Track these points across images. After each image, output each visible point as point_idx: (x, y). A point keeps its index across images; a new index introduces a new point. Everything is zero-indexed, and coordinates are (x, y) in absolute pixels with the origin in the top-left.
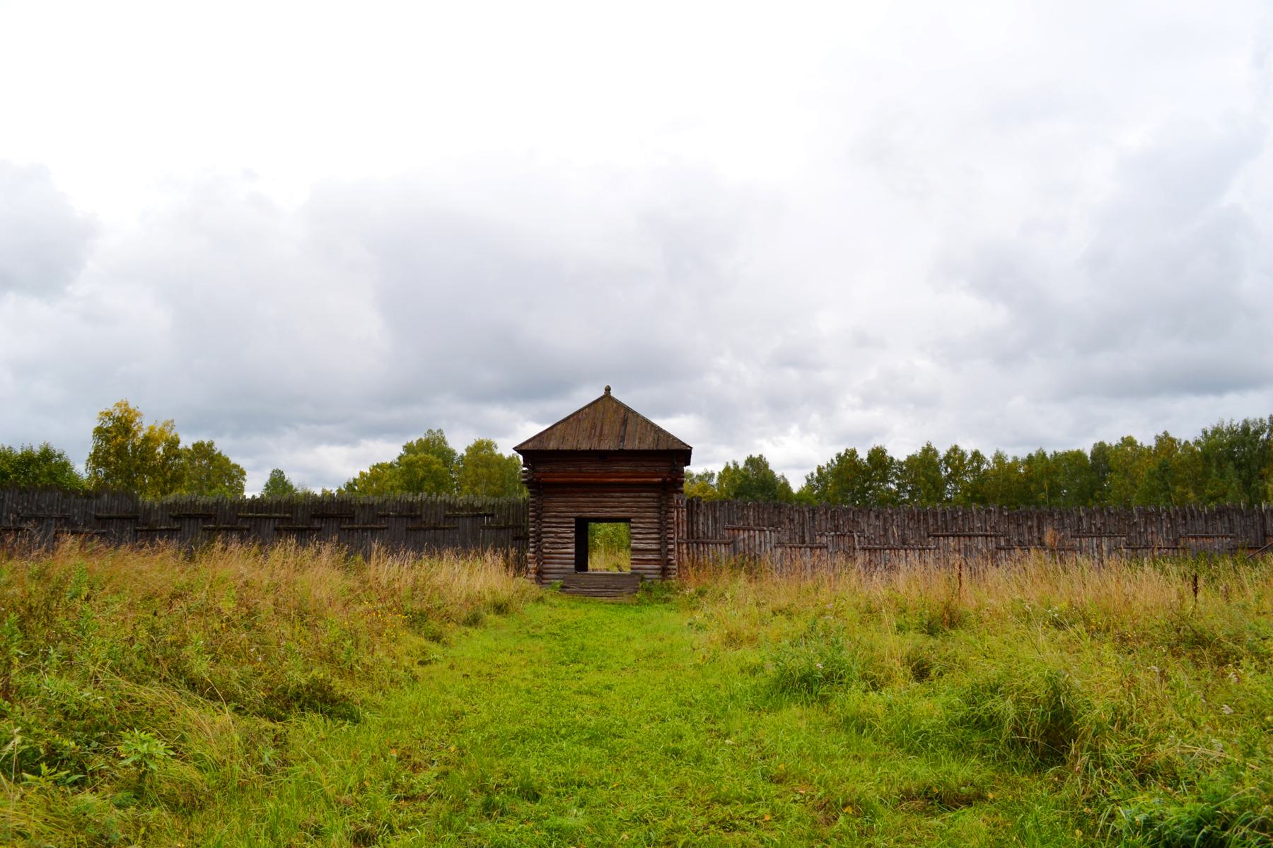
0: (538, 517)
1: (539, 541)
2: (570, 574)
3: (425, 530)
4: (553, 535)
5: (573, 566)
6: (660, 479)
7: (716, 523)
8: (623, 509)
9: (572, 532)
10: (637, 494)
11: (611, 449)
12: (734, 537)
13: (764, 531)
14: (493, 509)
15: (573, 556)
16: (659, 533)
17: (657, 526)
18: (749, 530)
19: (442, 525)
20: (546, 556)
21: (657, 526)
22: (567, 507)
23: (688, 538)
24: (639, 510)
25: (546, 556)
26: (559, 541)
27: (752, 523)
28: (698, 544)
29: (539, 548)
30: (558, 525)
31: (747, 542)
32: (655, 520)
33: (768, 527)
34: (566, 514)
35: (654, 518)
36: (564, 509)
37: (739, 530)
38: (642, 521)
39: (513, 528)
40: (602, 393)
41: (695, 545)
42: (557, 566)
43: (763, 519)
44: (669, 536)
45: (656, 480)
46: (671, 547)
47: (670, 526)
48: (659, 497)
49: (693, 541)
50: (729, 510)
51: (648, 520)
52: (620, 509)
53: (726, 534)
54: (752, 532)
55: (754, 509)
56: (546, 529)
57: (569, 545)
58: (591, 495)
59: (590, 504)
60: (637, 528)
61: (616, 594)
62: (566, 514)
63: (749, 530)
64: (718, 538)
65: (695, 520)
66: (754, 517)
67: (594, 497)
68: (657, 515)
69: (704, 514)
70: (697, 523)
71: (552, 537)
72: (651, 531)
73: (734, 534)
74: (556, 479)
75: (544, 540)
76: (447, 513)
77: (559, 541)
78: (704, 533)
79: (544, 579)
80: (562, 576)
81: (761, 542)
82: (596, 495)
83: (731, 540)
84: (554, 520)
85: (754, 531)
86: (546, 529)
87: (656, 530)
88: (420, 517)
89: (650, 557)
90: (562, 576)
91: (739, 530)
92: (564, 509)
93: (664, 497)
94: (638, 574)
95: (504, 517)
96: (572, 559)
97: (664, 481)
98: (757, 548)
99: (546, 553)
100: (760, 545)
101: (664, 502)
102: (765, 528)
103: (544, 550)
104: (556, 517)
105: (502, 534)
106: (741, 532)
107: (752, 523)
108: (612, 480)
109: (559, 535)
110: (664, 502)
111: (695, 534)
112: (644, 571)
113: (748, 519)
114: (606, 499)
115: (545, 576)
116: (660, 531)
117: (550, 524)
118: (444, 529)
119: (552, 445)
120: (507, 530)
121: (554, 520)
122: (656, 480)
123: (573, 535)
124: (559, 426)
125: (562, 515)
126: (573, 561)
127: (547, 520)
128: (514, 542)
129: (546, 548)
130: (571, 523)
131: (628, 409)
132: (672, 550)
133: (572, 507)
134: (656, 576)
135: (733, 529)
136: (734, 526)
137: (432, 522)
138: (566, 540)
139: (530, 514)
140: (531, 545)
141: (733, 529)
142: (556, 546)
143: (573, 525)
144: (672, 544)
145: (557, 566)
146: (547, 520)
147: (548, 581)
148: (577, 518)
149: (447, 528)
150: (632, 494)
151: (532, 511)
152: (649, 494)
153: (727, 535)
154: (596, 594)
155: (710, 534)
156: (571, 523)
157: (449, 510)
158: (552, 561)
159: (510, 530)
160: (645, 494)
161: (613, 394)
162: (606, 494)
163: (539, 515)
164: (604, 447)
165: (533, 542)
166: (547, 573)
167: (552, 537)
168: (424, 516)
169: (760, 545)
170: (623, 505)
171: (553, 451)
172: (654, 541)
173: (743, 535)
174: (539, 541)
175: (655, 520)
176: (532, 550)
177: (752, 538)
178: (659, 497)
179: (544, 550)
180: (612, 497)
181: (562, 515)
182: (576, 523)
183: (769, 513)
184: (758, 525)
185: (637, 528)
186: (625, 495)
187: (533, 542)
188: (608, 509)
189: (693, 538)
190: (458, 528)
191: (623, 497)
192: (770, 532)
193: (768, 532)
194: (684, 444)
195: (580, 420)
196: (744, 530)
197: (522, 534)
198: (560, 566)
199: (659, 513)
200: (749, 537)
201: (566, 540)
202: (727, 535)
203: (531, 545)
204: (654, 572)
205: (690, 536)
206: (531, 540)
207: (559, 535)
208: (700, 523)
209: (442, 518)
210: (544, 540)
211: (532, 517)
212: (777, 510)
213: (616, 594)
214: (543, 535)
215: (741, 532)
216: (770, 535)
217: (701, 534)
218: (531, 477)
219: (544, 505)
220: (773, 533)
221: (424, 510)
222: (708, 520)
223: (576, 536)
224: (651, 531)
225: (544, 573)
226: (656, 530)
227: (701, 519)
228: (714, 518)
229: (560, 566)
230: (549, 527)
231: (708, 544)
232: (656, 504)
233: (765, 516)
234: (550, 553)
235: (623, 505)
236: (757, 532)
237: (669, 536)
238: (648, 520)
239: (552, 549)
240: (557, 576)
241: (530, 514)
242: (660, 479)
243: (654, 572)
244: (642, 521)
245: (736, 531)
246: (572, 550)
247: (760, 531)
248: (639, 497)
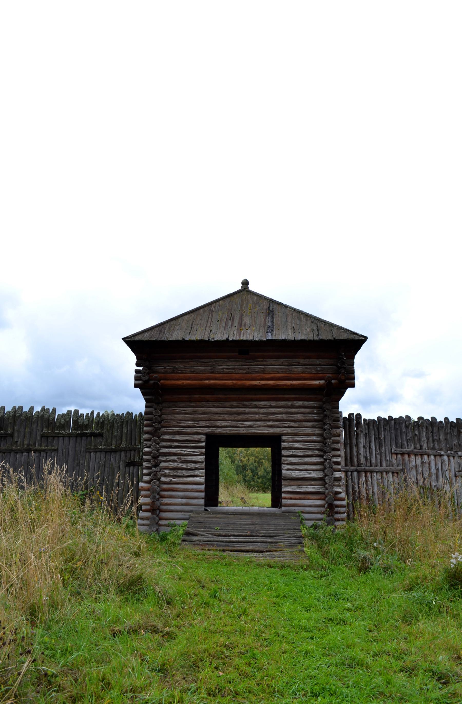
0: (154, 433)
1: (156, 466)
2: (198, 512)
3: (16, 452)
4: (175, 458)
5: (202, 502)
6: (322, 382)
7: (381, 446)
8: (271, 423)
9: (201, 454)
10: (290, 403)
11: (256, 339)
12: (404, 464)
13: (441, 455)
14: (102, 427)
15: (203, 487)
16: (321, 456)
17: (318, 446)
18: (422, 455)
19: (37, 447)
20: (165, 486)
21: (318, 446)
22: (193, 420)
23: (346, 465)
24: (292, 424)
25: (165, 486)
26: (183, 466)
27: (425, 446)
28: (359, 472)
29: (155, 475)
30: (182, 444)
31: (420, 470)
32: (315, 438)
33: (446, 451)
34: (194, 430)
35: (314, 435)
36: (191, 423)
37: (409, 455)
38: (298, 438)
39: (126, 452)
40: (238, 287)
41: (355, 474)
42: (179, 500)
43: (439, 441)
44: (334, 459)
45: (317, 382)
46: (337, 475)
47: (335, 446)
48: (320, 407)
49: (352, 468)
50: (396, 430)
51: (305, 438)
52: (268, 423)
53: (393, 459)
54: (426, 457)
55: (427, 428)
56: (165, 450)
57: (198, 479)
58: (228, 404)
59: (226, 417)
60: (291, 448)
61: (269, 547)
62: (194, 430)
63: (422, 455)
64: (384, 464)
65: (354, 442)
66: (428, 439)
67: (231, 407)
68: (318, 431)
69: (365, 435)
70: (357, 445)
71: (174, 461)
72: (310, 453)
73: (403, 460)
74: (181, 382)
75: (163, 464)
76: (45, 431)
77: (183, 466)
78: (366, 459)
79: (161, 519)
80: (187, 515)
81: (437, 470)
82: (234, 403)
83: (401, 467)
84: (177, 437)
85: (429, 455)
86: (165, 450)
87: (316, 452)
88: (12, 435)
89: (309, 489)
90: (187, 515)
91: (409, 455)
92: (191, 423)
93: (326, 406)
94: (295, 513)
95: (116, 437)
96: (285, 448)
97: (329, 384)
98: (434, 477)
99: (165, 483)
100: (437, 474)
101: (327, 412)
102: (443, 453)
103: (163, 479)
104: (179, 433)
105: (112, 459)
106: (413, 457)
107: (425, 446)
108: (257, 382)
109: (183, 458)
110: (327, 412)
111: (355, 460)
112: (302, 509)
113: (420, 440)
114: (248, 410)
115: (163, 515)
116: (323, 452)
117: (171, 443)
118: (40, 451)
119: (177, 335)
120: (118, 454)
121: (177, 437)
122: (317, 382)
123: (202, 458)
124: (186, 317)
125: (188, 430)
126: (203, 494)
127: (167, 437)
128: (127, 469)
129: (166, 476)
130: (199, 441)
131: (272, 301)
132: (339, 479)
133: (201, 420)
134: (319, 516)
135: (403, 454)
136: (404, 450)
137: (26, 442)
138: (193, 465)
139: (145, 429)
140: (145, 471)
141: (403, 454)
142: (178, 473)
143: (203, 444)
144: (339, 471)
145: (179, 500)
146: (167, 437)
147: (166, 522)
148: (206, 434)
149: (44, 451)
150: (282, 403)
151: (147, 426)
152: (306, 403)
153: (394, 461)
154: (238, 547)
155: (374, 460)
156: (199, 441)
157: (47, 427)
158: (349, 458)
159: (123, 453)
160: (300, 403)
161: (251, 287)
162: (247, 403)
163: (157, 430)
164: (247, 336)
165: (147, 468)
166: (314, 407)
167: (174, 461)
168: (16, 435)
169: (437, 474)
170: (271, 417)
171: (177, 342)
172: (314, 467)
173: (415, 461)
174: (156, 466)
175: (315, 438)
176: (146, 478)
177: (427, 465)
178: (320, 407)
179: (163, 479)
180: (256, 407)
181: (188, 430)
182: (207, 441)
183: (446, 434)
184: (434, 448)
185: (291, 448)
186: (273, 404)
187: (147, 468)
188: (251, 423)
189: (352, 466)
190: (57, 450)
191: (271, 407)
192: (448, 456)
193: (446, 458)
194: (356, 334)
195: (213, 311)
196: (416, 455)
197: (137, 459)
198: (184, 501)
199: (322, 428)
200: (423, 463)
201: (193, 465)
202: (394, 461)
203: (145, 471)
204: (316, 509)
205: (349, 464)
206: (145, 464)
207: (183, 458)
208: (361, 446)
209: (38, 438)
210: (163, 464)
211: (147, 433)
212: (456, 430)
213: (269, 547)
214: (161, 458)
215: (413, 457)
216: (449, 460)
217: (363, 460)
218: (147, 378)
219: (164, 417)
220: (452, 458)
221: (16, 428)
222: (370, 442)
223: (207, 460)
224: (310, 453)
225: (161, 511)
226: (316, 452)
227: (362, 441)
228: (378, 439)
229: (184, 501)
230: (170, 447)
231: (371, 472)
232: (315, 417)
233: (442, 437)
234: (170, 483)
235: (271, 417)
236: (432, 457)
237: (334, 459)
238: (305, 438)
239: (174, 477)
240: (179, 515)
241: (145, 429)
242: (322, 382)
243: (316, 509)
244: (298, 438)
245: (406, 456)
246: (202, 479)
247: (435, 456)
248: (292, 407)
